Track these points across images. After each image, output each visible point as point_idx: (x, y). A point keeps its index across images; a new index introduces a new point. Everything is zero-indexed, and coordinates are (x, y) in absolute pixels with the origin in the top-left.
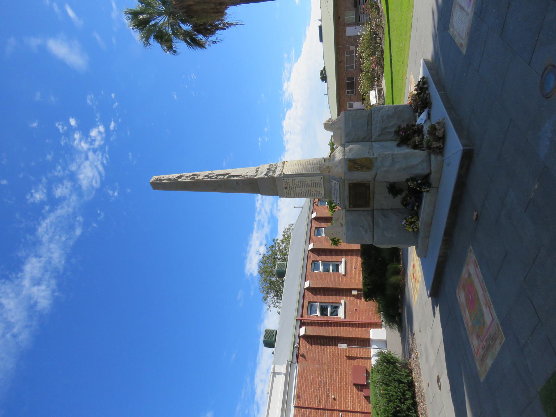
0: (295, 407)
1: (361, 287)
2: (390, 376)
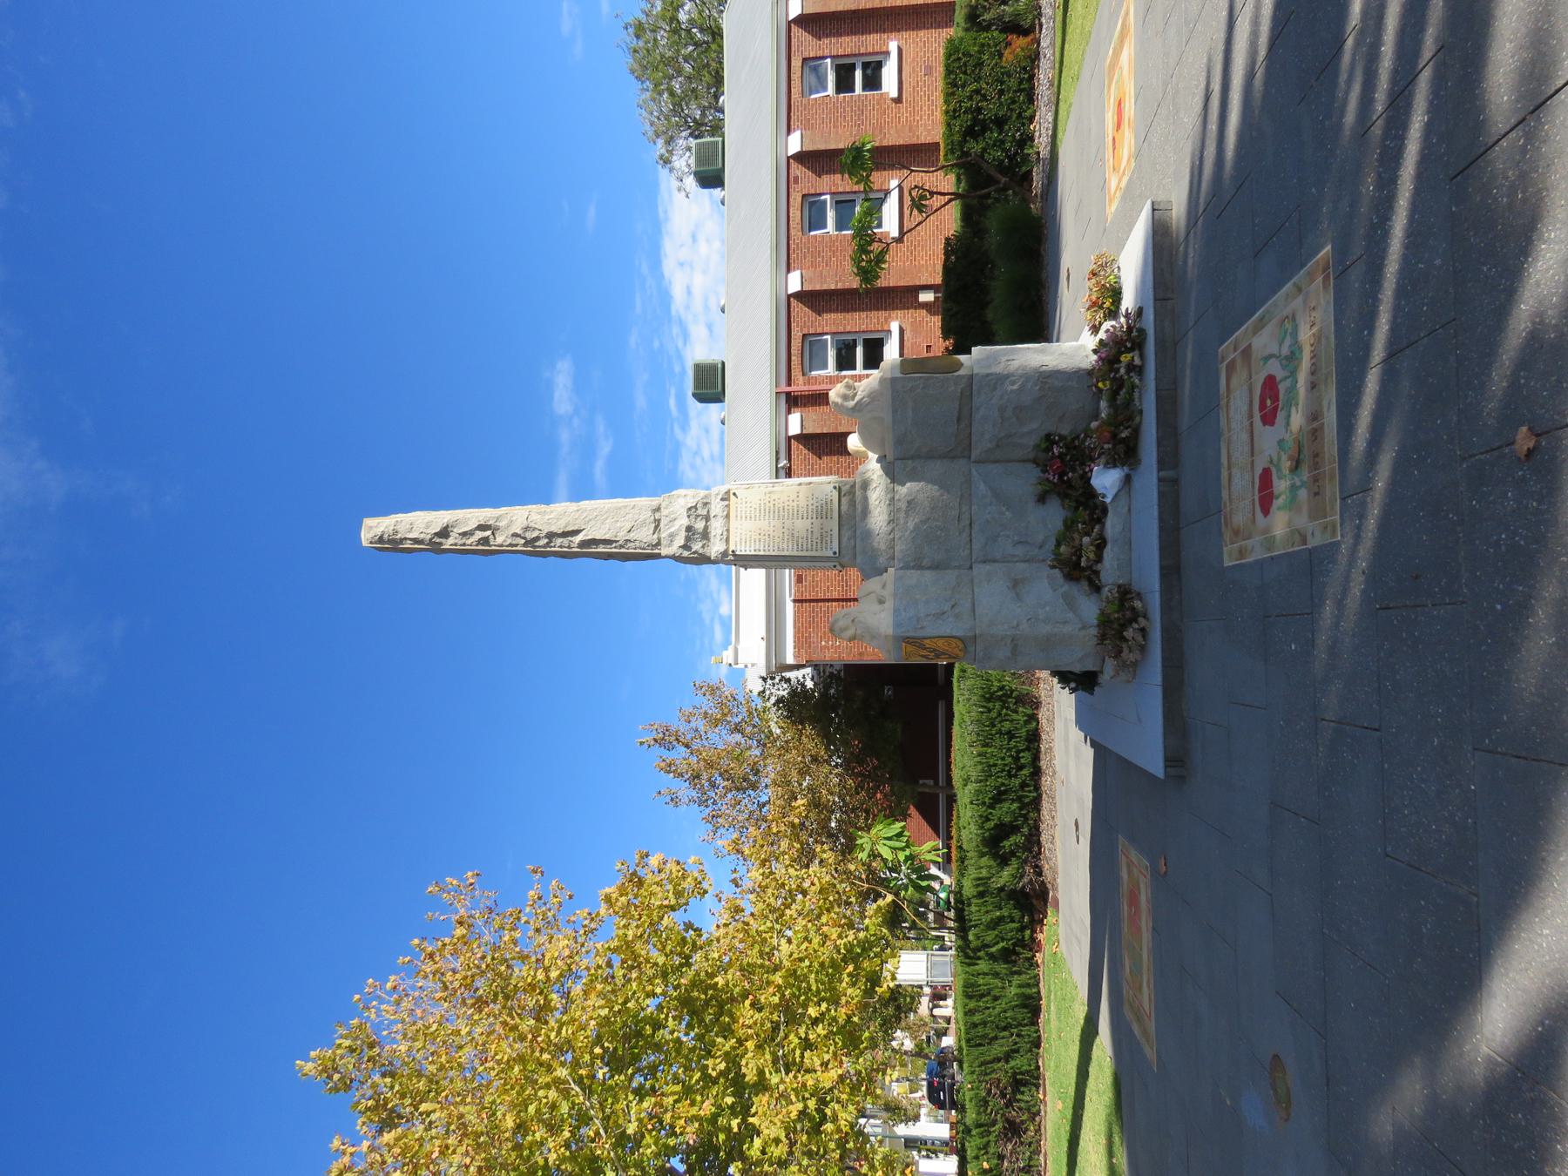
0: (795, 601)
1: (953, 189)
2: (993, 725)
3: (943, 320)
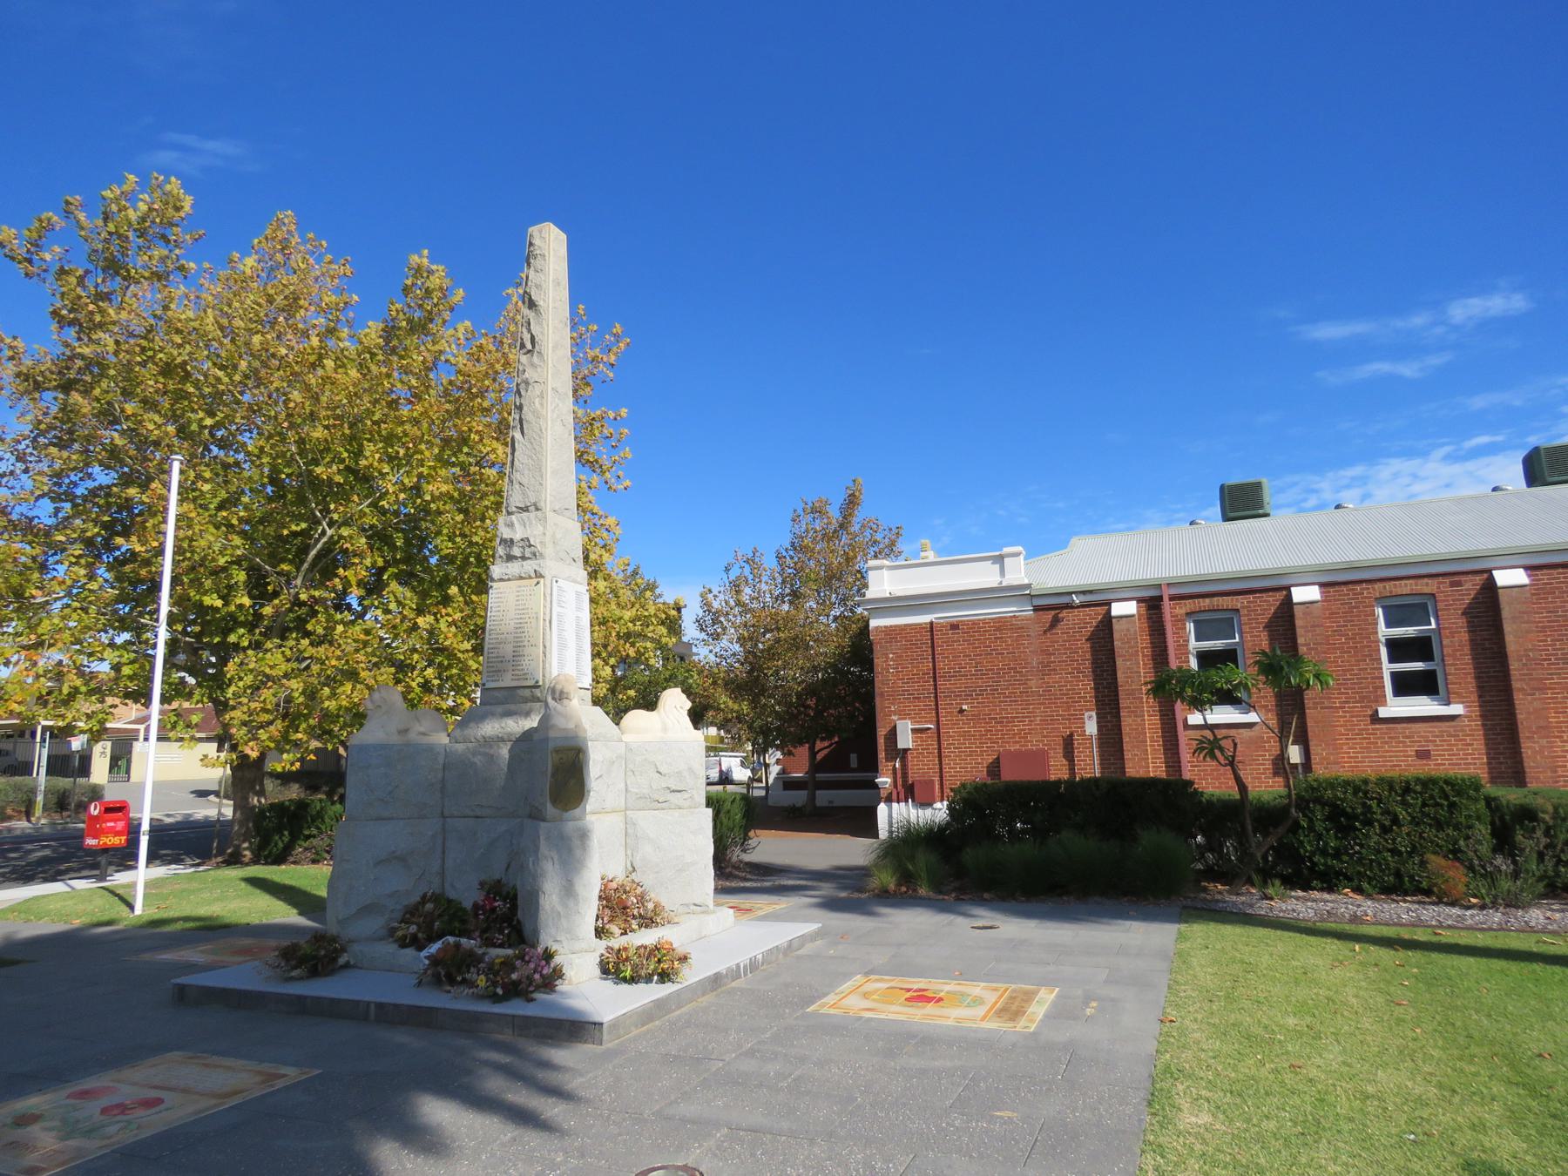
3: (1095, 781)
